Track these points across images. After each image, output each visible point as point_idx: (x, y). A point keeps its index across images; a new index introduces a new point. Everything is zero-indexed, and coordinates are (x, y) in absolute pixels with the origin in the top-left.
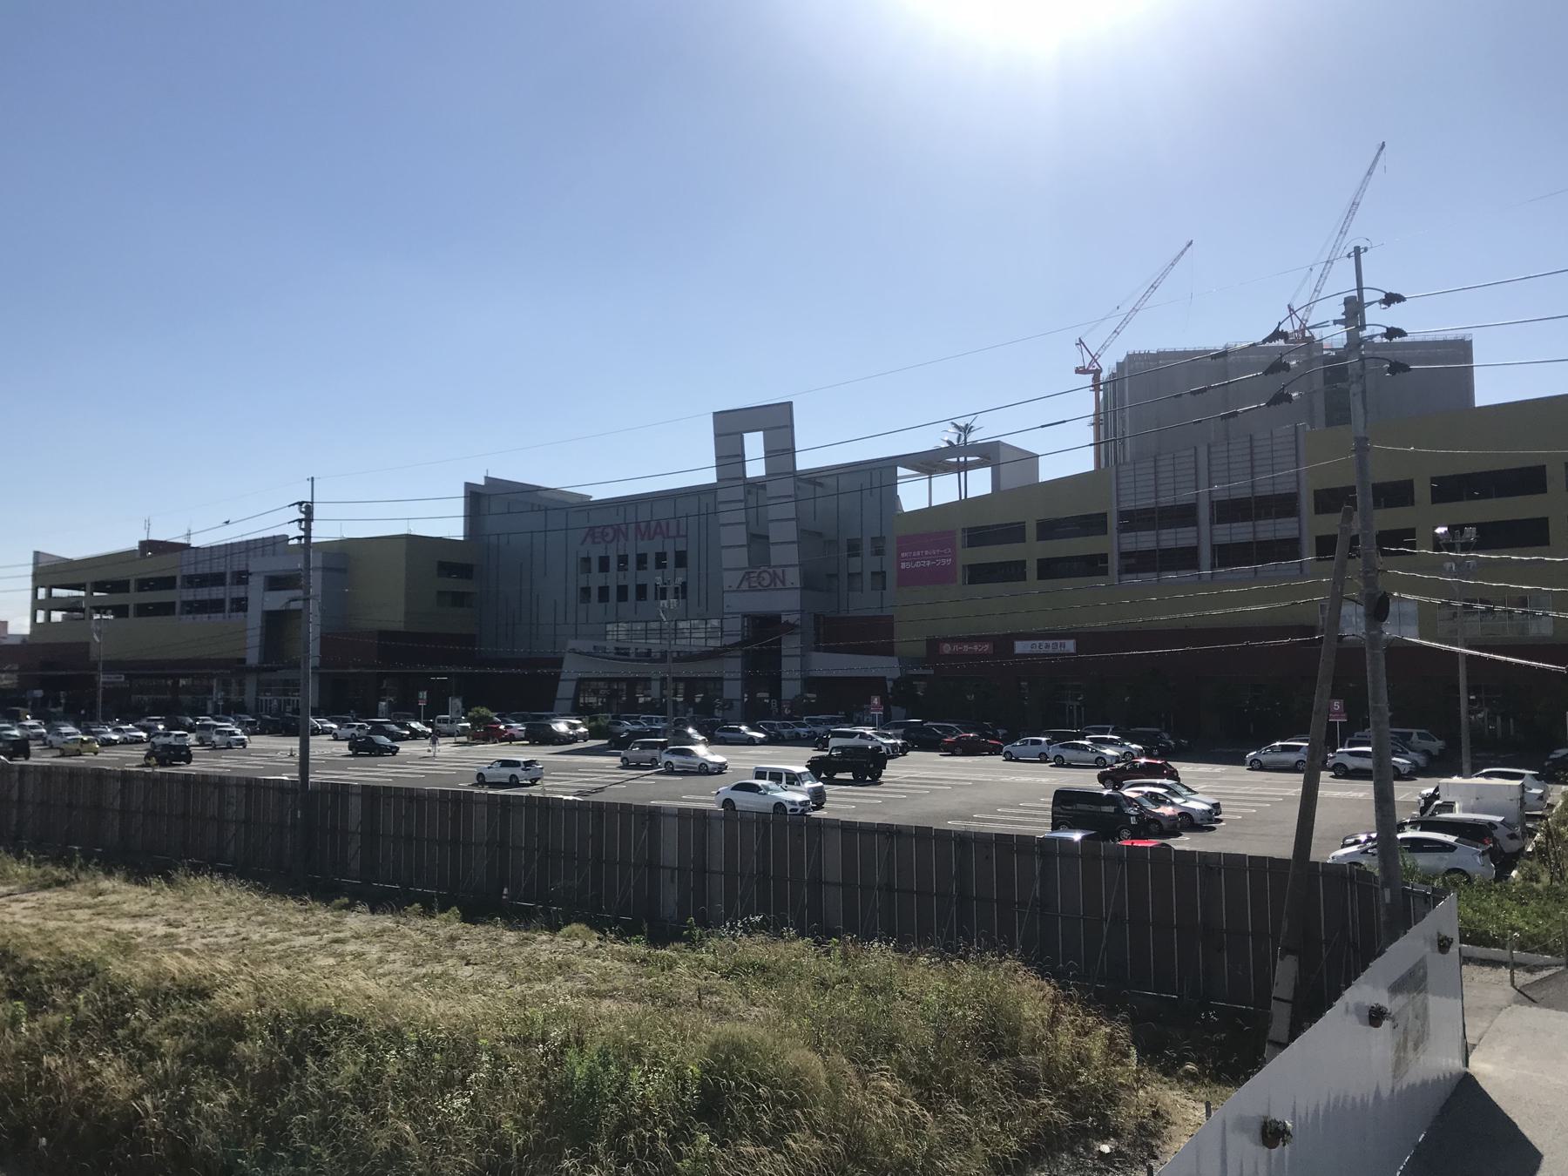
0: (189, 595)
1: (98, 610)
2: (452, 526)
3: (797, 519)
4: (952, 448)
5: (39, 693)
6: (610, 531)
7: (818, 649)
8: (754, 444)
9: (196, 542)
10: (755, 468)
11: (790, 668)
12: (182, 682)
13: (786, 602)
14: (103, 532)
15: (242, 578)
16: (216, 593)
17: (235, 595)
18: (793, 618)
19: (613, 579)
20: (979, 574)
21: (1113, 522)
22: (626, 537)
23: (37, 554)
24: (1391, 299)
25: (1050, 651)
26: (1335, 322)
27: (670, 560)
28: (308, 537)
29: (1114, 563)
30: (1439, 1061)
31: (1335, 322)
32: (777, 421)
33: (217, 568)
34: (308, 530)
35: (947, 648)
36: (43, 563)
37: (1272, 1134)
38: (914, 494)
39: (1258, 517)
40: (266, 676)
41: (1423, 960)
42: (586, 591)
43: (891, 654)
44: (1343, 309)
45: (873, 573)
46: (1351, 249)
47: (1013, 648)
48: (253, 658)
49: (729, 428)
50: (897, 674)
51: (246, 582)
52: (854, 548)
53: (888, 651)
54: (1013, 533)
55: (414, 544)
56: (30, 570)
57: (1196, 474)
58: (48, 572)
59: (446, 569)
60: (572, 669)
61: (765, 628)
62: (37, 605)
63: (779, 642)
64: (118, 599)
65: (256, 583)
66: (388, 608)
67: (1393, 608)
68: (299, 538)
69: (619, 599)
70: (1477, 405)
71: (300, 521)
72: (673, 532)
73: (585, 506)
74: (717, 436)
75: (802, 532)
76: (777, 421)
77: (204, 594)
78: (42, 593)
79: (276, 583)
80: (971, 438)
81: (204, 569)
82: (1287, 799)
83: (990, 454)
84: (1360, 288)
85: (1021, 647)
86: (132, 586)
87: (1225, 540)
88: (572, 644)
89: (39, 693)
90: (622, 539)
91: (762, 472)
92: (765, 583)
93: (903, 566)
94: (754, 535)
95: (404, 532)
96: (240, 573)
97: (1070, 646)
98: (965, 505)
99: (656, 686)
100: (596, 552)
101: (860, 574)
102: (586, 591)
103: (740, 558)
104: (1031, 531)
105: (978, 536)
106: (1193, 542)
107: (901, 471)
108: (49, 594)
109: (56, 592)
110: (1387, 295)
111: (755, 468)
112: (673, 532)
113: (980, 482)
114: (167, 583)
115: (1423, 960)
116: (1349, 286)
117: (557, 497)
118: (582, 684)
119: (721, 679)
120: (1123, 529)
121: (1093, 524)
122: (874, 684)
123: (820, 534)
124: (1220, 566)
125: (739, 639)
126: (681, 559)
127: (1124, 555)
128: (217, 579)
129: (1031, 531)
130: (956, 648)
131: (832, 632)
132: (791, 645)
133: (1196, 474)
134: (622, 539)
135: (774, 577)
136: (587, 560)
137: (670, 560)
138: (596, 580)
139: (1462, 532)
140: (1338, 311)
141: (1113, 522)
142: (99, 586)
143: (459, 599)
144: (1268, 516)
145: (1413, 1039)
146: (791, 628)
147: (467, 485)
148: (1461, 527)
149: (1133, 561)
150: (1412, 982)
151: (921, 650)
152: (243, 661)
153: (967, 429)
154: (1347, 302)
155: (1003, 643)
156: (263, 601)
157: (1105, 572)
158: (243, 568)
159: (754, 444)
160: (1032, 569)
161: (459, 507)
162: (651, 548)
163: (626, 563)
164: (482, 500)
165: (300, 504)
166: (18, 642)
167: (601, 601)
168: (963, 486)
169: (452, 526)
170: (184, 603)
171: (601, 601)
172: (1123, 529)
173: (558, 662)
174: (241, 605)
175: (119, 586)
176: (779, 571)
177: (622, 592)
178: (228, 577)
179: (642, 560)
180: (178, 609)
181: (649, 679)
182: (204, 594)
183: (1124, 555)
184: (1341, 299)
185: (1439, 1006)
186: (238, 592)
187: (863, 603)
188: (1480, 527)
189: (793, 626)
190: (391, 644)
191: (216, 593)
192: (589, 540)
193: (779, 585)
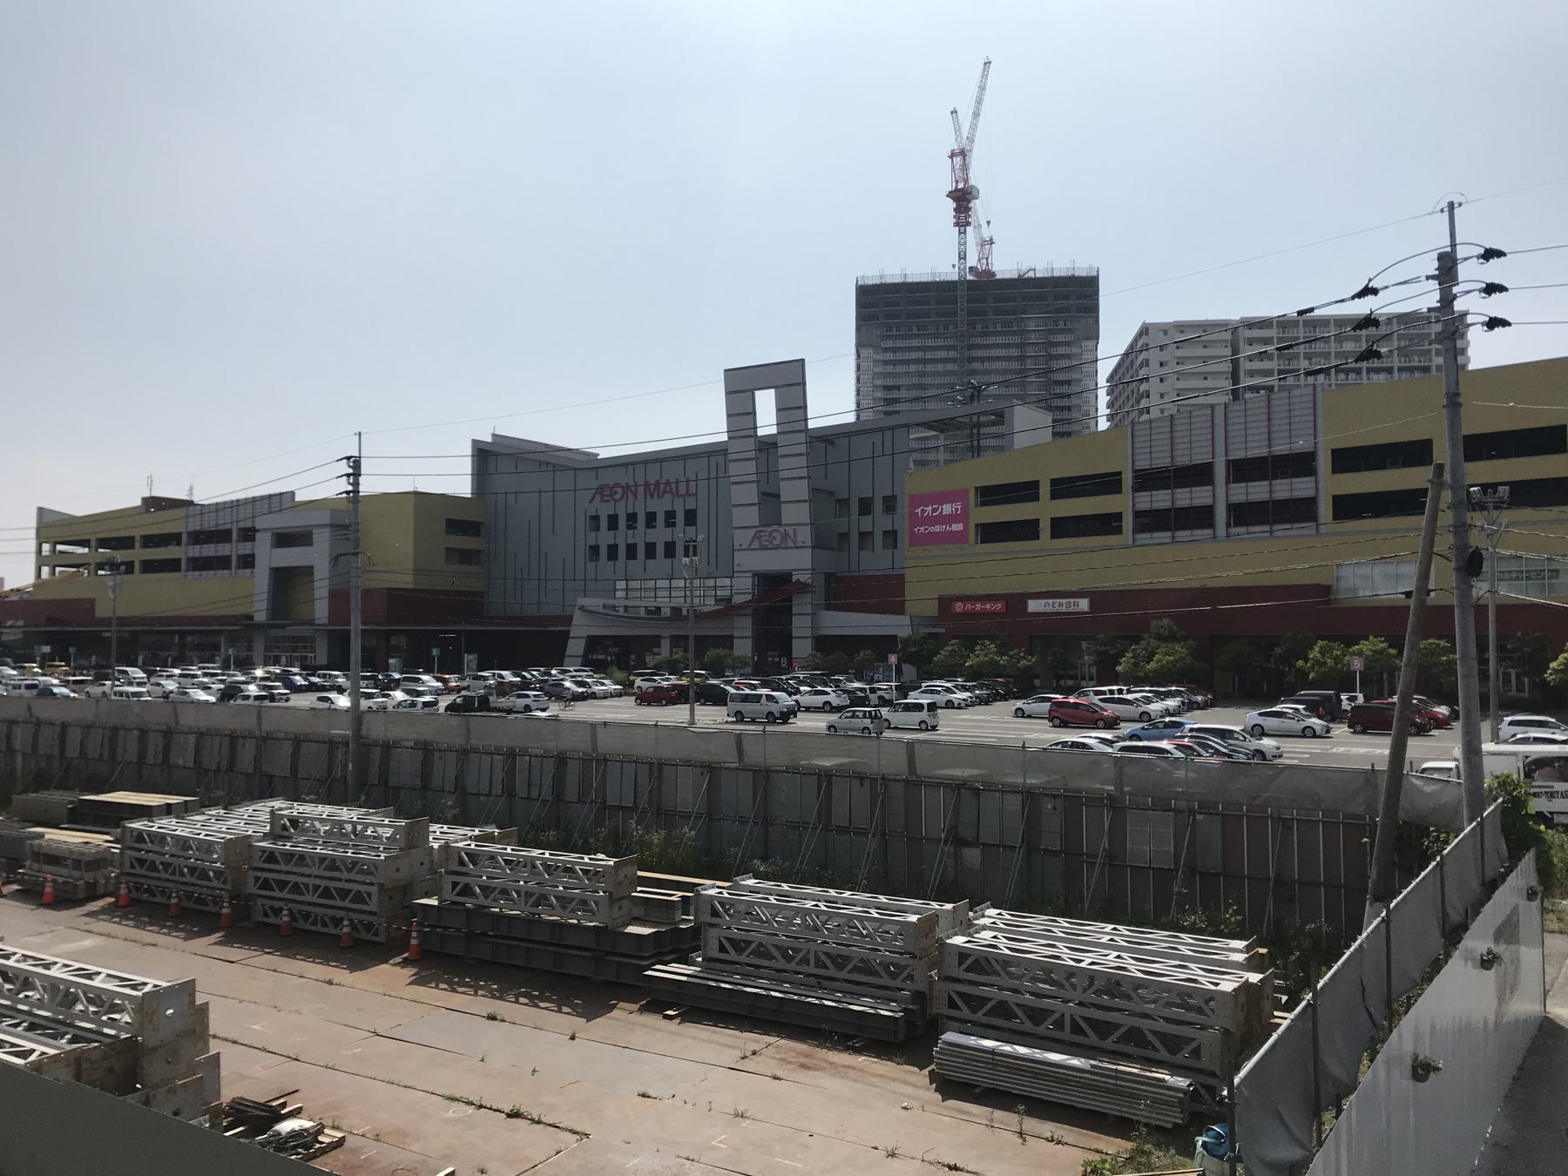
0: (196, 551)
2: (460, 484)
3: (809, 477)
5: (46, 649)
6: (620, 490)
7: (828, 608)
8: (766, 406)
9: (198, 498)
11: (801, 627)
12: (189, 639)
13: (798, 561)
14: (105, 488)
15: (249, 534)
16: (223, 549)
17: (190, 555)
18: (804, 578)
19: (622, 537)
20: (991, 533)
21: (1128, 481)
22: (635, 495)
23: (41, 510)
24: (1490, 254)
25: (1064, 609)
26: (1428, 278)
27: (680, 519)
28: (356, 491)
30: (1524, 1006)
31: (1428, 278)
33: (224, 522)
34: (356, 484)
35: (959, 607)
36: (47, 519)
37: (1422, 1070)
39: (1275, 478)
40: (273, 632)
41: (1516, 907)
42: (594, 550)
44: (1436, 264)
46: (1444, 204)
47: (1091, 605)
48: (261, 617)
51: (253, 539)
53: (899, 609)
55: (421, 499)
56: (33, 523)
57: (1213, 427)
58: (51, 527)
59: (454, 526)
60: (581, 629)
61: (775, 587)
62: (41, 561)
63: (790, 600)
64: (120, 556)
65: (264, 540)
66: (396, 561)
67: (1486, 567)
68: (348, 492)
69: (628, 558)
71: (348, 475)
72: (682, 490)
74: (728, 393)
75: (814, 490)
77: (209, 550)
78: (46, 547)
79: (284, 539)
81: (209, 524)
82: (1381, 756)
84: (1453, 245)
85: (1034, 606)
87: (1242, 498)
88: (581, 601)
89: (46, 649)
90: (631, 498)
91: (773, 430)
92: (777, 542)
94: (765, 494)
95: (411, 489)
96: (246, 530)
97: (1083, 604)
99: (666, 644)
100: (605, 510)
101: (871, 533)
102: (594, 550)
103: (752, 516)
106: (1208, 501)
108: (54, 550)
109: (60, 547)
110: (1487, 251)
112: (682, 490)
114: (173, 539)
115: (1516, 907)
116: (1444, 243)
117: (578, 457)
118: (593, 643)
120: (1137, 488)
122: (883, 644)
123: (831, 493)
124: (1236, 525)
125: (749, 597)
126: (691, 517)
128: (222, 536)
130: (969, 606)
131: (843, 591)
132: (802, 607)
133: (1213, 427)
134: (631, 498)
135: (785, 536)
137: (680, 519)
138: (605, 538)
139: (1495, 492)
140: (1432, 267)
141: (1128, 481)
142: (103, 543)
143: (466, 557)
144: (1284, 475)
145: (1506, 989)
146: (803, 588)
147: (474, 441)
148: (1495, 486)
149: (1147, 520)
150: (1508, 931)
151: (932, 609)
152: (251, 617)
154: (1441, 257)
155: (1016, 602)
156: (269, 557)
157: (1119, 531)
158: (249, 524)
159: (766, 406)
160: (1045, 526)
161: (466, 465)
162: (660, 506)
164: (489, 457)
165: (348, 458)
167: (610, 558)
169: (460, 484)
171: (610, 558)
172: (1137, 488)
173: (568, 620)
174: (248, 562)
175: (125, 543)
176: (790, 530)
177: (651, 550)
178: (184, 537)
179: (651, 518)
180: (183, 566)
182: (209, 550)
183: (1138, 514)
184: (1435, 255)
185: (1529, 955)
186: (245, 548)
187: (874, 561)
188: (1514, 485)
189: (805, 585)
190: (398, 603)
191: (223, 549)
192: (598, 497)
193: (791, 544)
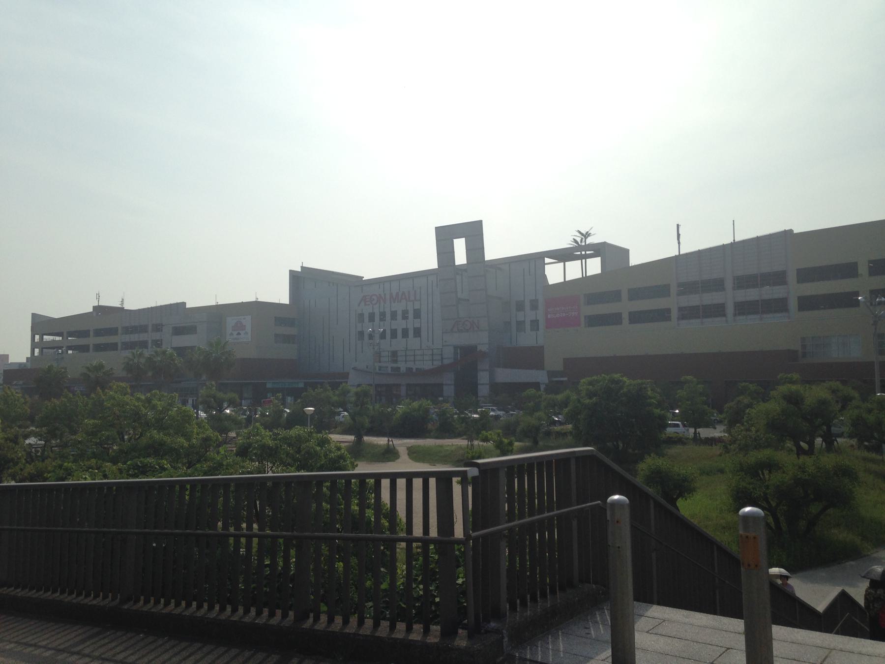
1: (69, 348)
4: (578, 247)
8: (460, 247)
10: (461, 257)
29: (675, 314)
32: (473, 232)
38: (554, 273)
43: (543, 369)
45: (531, 321)
49: (445, 236)
50: (547, 381)
52: (520, 306)
54: (615, 296)
58: (40, 325)
62: (34, 346)
70: (288, 303)
72: (412, 298)
73: (355, 282)
76: (473, 232)
80: (589, 241)
83: (601, 250)
86: (91, 333)
91: (551, 281)
93: (549, 316)
98: (585, 280)
104: (625, 295)
105: (594, 298)
107: (547, 260)
111: (461, 257)
112: (412, 298)
113: (594, 266)
114: (112, 331)
119: (442, 384)
121: (663, 291)
127: (680, 309)
128: (143, 329)
129: (625, 295)
136: (361, 315)
142: (71, 334)
153: (587, 235)
159: (460, 247)
162: (399, 307)
163: (385, 316)
164: (301, 280)
166: (16, 368)
168: (584, 268)
170: (124, 343)
179: (394, 315)
181: (400, 385)
183: (680, 309)
186: (157, 336)
192: (363, 303)
